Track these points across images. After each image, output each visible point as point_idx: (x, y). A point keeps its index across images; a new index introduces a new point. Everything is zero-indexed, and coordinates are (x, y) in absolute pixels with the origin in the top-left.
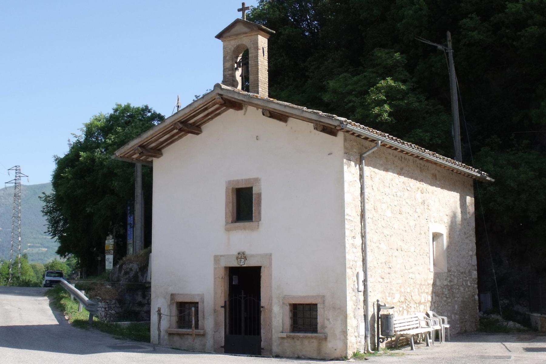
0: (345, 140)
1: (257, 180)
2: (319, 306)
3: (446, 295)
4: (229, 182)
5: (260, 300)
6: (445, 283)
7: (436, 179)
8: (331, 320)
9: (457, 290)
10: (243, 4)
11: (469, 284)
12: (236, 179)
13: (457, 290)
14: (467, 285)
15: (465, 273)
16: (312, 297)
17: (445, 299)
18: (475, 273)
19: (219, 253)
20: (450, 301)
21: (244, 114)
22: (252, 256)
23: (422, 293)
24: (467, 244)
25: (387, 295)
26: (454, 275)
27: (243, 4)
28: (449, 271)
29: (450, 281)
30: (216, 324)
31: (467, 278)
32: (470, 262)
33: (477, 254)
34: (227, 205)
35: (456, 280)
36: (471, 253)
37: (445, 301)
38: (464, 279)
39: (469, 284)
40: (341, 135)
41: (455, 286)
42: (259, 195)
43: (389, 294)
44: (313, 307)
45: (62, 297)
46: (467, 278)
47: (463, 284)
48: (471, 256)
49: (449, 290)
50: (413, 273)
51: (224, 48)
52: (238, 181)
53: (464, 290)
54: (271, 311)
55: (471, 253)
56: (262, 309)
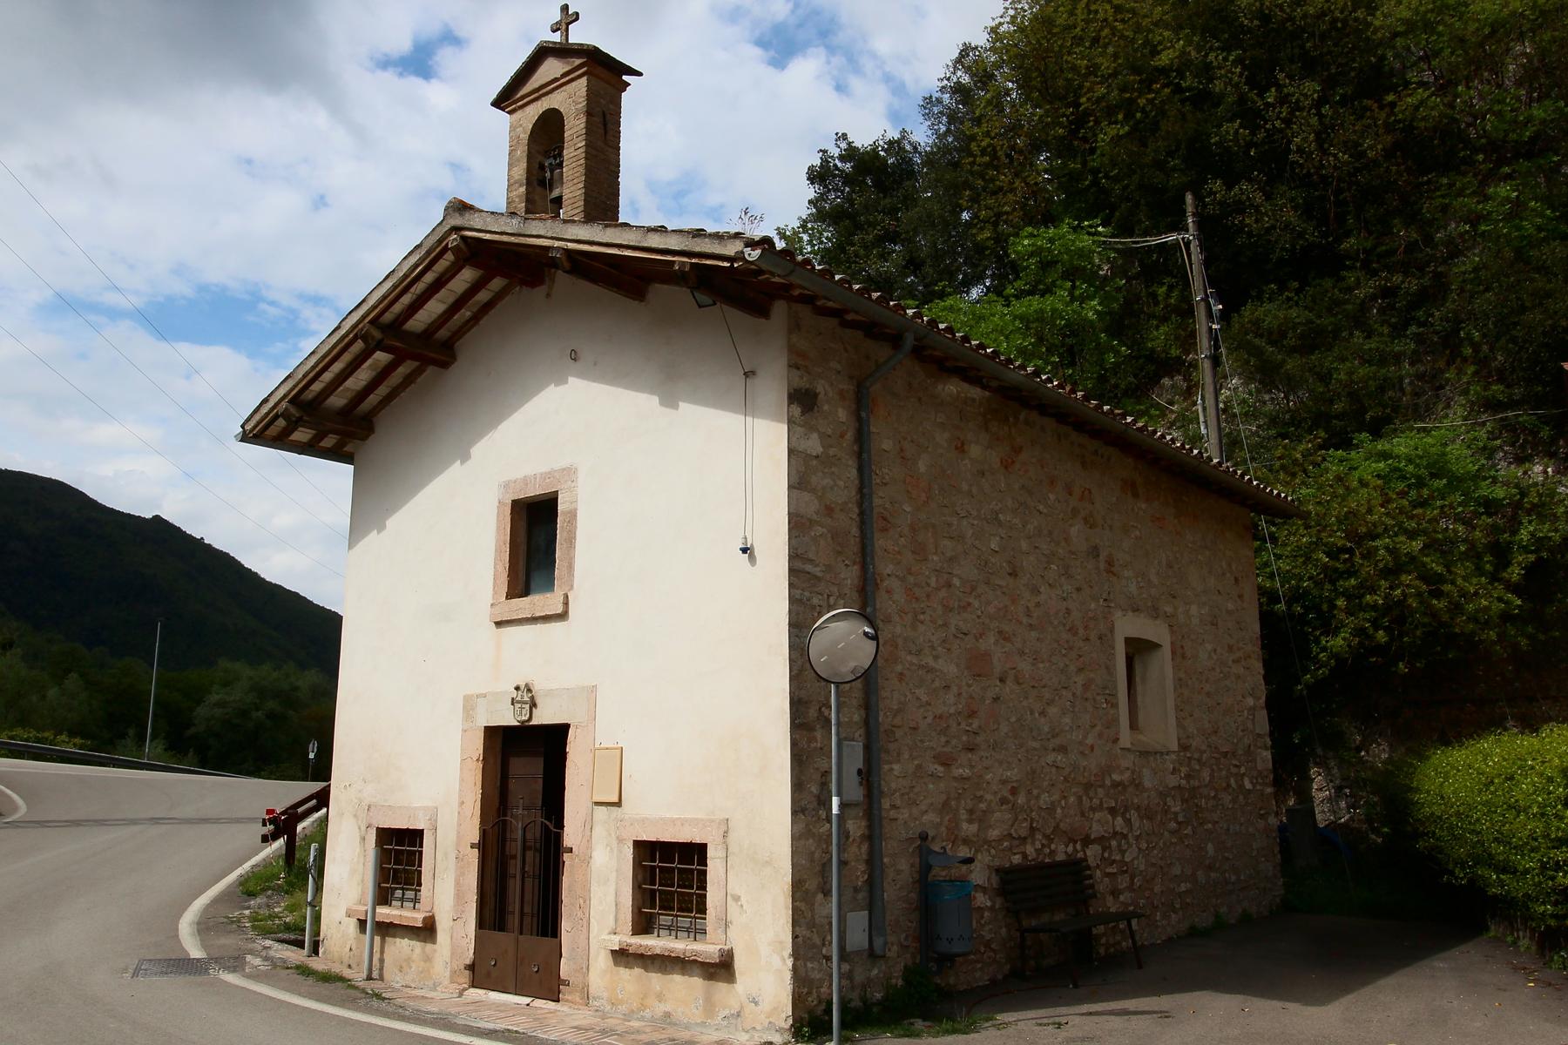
0: (795, 326)
1: (570, 472)
2: (711, 853)
3: (1176, 814)
4: (506, 485)
5: (562, 827)
6: (1173, 781)
7: (1136, 495)
8: (743, 900)
9: (1211, 803)
10: (565, 8)
11: (1248, 786)
12: (519, 475)
13: (1211, 803)
14: (1241, 786)
15: (1234, 754)
16: (694, 822)
17: (1173, 825)
18: (1267, 754)
19: (474, 690)
20: (1188, 831)
21: (548, 295)
22: (550, 693)
23: (1093, 809)
24: (1238, 677)
25: (963, 815)
26: (1199, 761)
27: (565, 8)
28: (1184, 747)
29: (1188, 777)
30: (459, 896)
31: (1243, 770)
32: (1250, 726)
33: (1269, 705)
34: (498, 551)
35: (1206, 774)
36: (1250, 701)
37: (1173, 832)
38: (1234, 770)
39: (1248, 786)
40: (780, 309)
41: (1205, 791)
42: (573, 515)
43: (971, 812)
44: (696, 852)
45: (1328, 769)
46: (1243, 770)
47: (1229, 785)
48: (1252, 709)
49: (1184, 801)
50: (1062, 749)
51: (513, 128)
52: (525, 480)
53: (1234, 801)
54: (587, 860)
55: (1250, 701)
56: (566, 856)
